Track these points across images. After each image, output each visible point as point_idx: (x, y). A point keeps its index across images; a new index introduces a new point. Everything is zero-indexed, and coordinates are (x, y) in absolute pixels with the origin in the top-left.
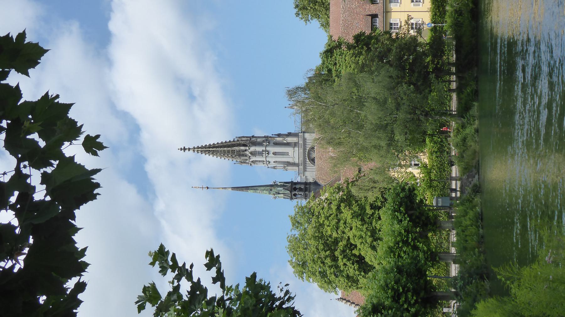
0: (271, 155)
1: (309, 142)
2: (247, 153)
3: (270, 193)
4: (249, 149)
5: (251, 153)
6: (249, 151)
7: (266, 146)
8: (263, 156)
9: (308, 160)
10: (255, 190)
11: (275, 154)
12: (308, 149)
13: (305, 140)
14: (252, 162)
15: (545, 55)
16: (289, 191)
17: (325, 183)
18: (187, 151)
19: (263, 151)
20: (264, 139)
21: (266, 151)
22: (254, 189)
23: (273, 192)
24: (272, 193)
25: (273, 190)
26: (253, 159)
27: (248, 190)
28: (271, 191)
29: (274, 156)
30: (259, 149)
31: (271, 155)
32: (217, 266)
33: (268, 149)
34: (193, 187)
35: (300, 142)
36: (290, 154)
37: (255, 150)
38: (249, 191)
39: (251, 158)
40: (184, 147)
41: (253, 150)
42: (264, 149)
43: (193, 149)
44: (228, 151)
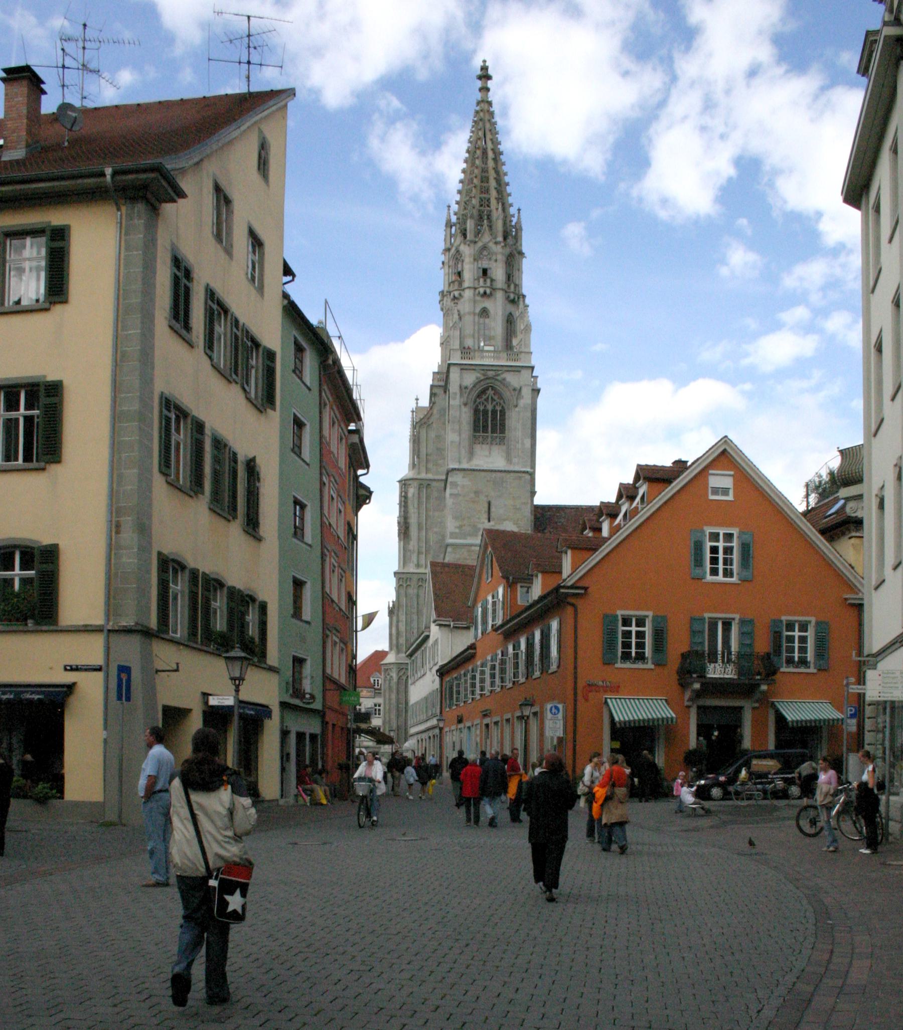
2: (486, 238)
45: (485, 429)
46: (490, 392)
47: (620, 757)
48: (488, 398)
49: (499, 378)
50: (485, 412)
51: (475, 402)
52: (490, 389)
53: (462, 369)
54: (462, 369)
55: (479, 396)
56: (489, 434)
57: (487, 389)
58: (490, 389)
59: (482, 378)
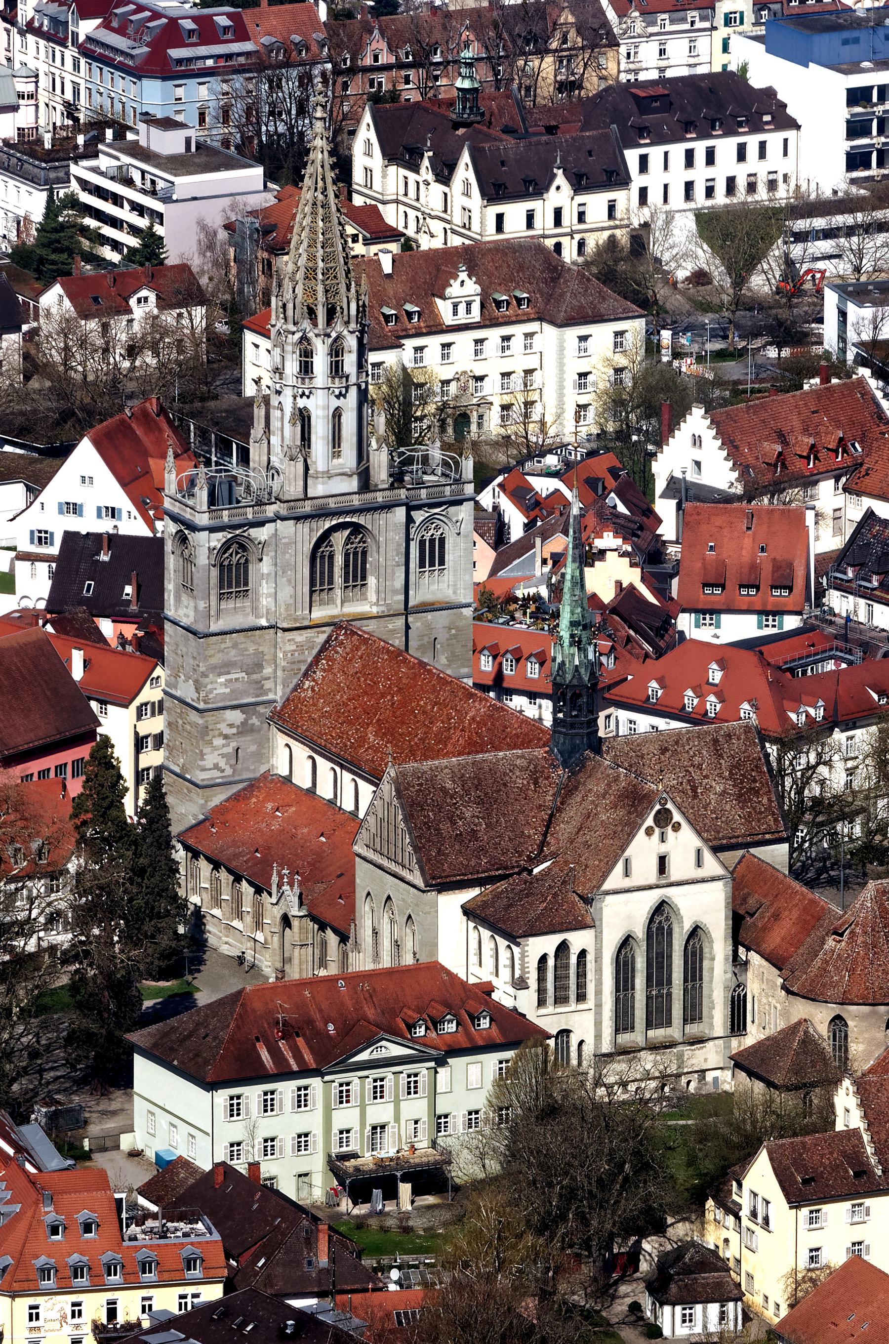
0: (335, 403)
2: (339, 327)
6: (345, 333)
9: (327, 525)
11: (337, 414)
13: (388, 507)
21: (347, 388)
30: (350, 363)
31: (335, 403)
32: (551, 1042)
36: (335, 461)
37: (346, 349)
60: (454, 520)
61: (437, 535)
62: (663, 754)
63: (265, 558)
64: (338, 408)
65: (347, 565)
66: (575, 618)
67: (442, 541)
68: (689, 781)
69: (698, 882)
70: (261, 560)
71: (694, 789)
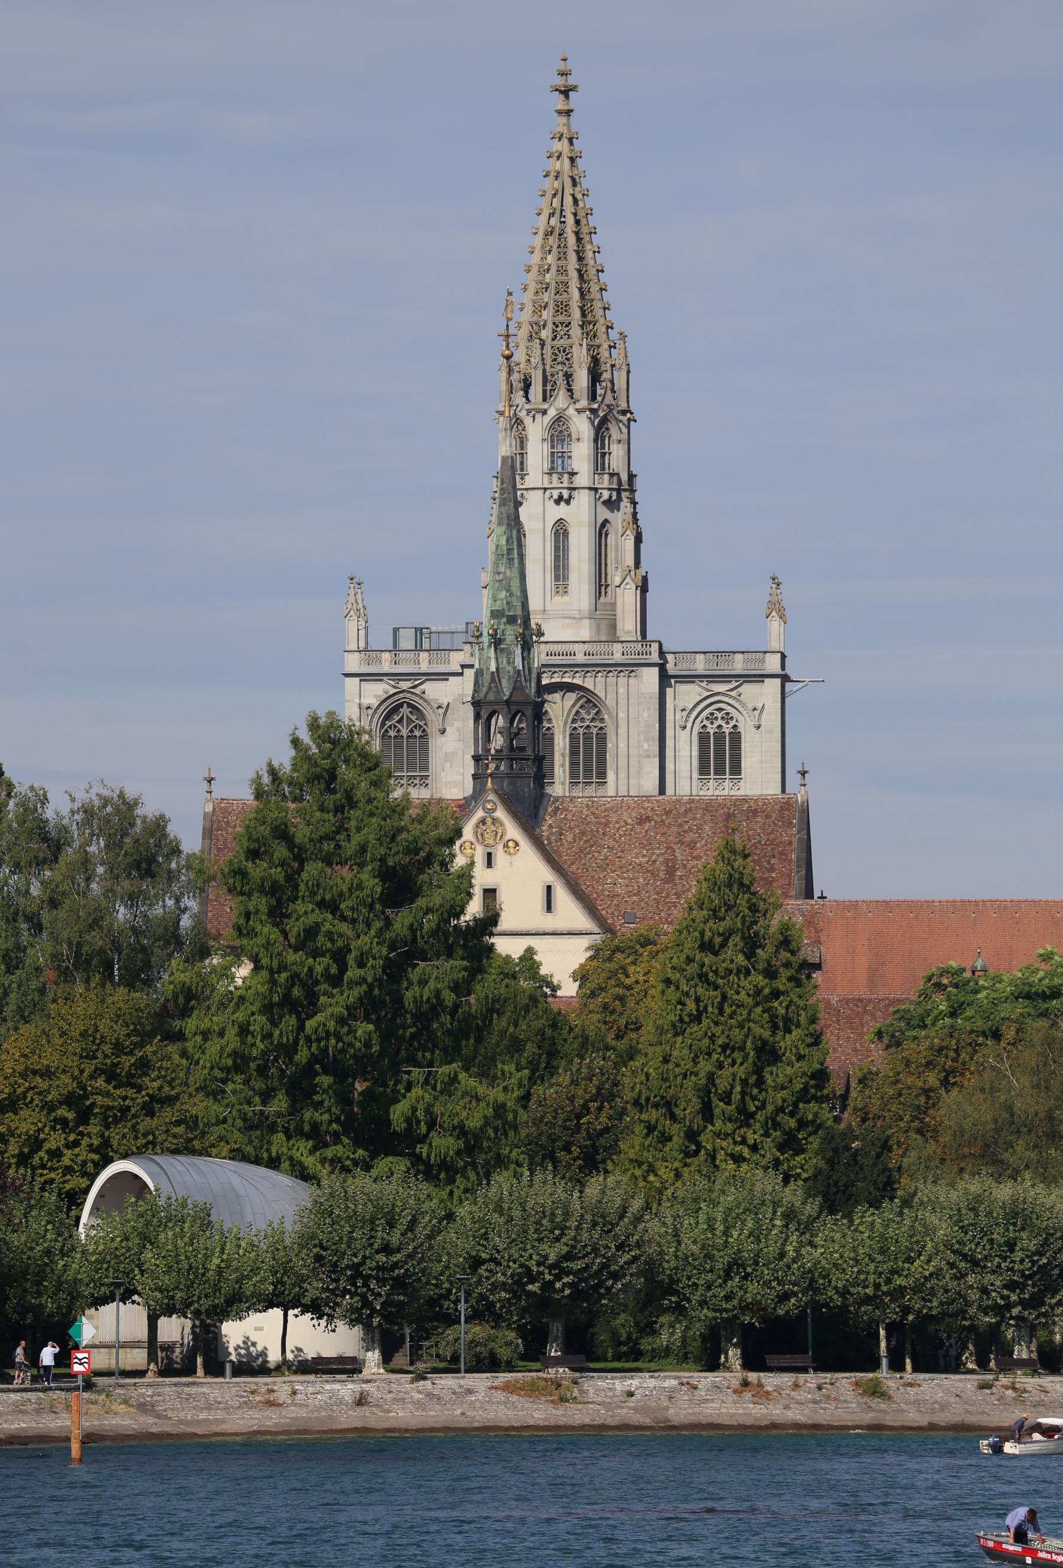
1: (621, 690)
2: (561, 400)
3: (495, 614)
4: (579, 411)
5: (560, 419)
6: (571, 411)
7: (596, 490)
8: (550, 474)
10: (508, 554)
11: (561, 532)
12: (588, 684)
13: (630, 667)
14: (519, 422)
15: (595, 361)
16: (511, 695)
17: (548, 839)
18: (560, 103)
19: (572, 474)
20: (624, 477)
22: (510, 551)
23: (502, 627)
24: (499, 624)
25: (509, 627)
26: (536, 430)
27: (508, 525)
28: (504, 620)
29: (550, 524)
30: (581, 455)
33: (583, 501)
34: (510, 294)
35: (617, 648)
36: (558, 598)
37: (574, 436)
38: (504, 528)
39: (539, 416)
40: (574, 88)
41: (573, 429)
42: (583, 479)
43: (569, 130)
44: (562, 308)
45: (720, 771)
46: (405, 710)
47: (318, 960)
48: (402, 717)
49: (417, 691)
50: (588, 737)
51: (383, 724)
52: (405, 705)
53: (361, 680)
54: (361, 680)
55: (388, 717)
56: (712, 776)
57: (401, 705)
58: (405, 705)
59: (393, 691)
60: (750, 706)
61: (727, 729)
62: (640, 824)
63: (449, 730)
64: (560, 521)
65: (574, 752)
66: (498, 606)
67: (736, 738)
68: (667, 861)
69: (554, 934)
70: (443, 732)
71: (671, 871)
